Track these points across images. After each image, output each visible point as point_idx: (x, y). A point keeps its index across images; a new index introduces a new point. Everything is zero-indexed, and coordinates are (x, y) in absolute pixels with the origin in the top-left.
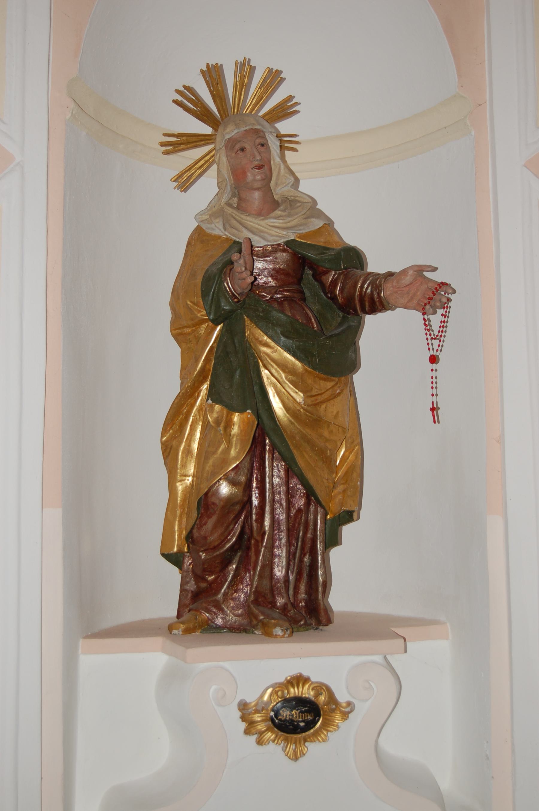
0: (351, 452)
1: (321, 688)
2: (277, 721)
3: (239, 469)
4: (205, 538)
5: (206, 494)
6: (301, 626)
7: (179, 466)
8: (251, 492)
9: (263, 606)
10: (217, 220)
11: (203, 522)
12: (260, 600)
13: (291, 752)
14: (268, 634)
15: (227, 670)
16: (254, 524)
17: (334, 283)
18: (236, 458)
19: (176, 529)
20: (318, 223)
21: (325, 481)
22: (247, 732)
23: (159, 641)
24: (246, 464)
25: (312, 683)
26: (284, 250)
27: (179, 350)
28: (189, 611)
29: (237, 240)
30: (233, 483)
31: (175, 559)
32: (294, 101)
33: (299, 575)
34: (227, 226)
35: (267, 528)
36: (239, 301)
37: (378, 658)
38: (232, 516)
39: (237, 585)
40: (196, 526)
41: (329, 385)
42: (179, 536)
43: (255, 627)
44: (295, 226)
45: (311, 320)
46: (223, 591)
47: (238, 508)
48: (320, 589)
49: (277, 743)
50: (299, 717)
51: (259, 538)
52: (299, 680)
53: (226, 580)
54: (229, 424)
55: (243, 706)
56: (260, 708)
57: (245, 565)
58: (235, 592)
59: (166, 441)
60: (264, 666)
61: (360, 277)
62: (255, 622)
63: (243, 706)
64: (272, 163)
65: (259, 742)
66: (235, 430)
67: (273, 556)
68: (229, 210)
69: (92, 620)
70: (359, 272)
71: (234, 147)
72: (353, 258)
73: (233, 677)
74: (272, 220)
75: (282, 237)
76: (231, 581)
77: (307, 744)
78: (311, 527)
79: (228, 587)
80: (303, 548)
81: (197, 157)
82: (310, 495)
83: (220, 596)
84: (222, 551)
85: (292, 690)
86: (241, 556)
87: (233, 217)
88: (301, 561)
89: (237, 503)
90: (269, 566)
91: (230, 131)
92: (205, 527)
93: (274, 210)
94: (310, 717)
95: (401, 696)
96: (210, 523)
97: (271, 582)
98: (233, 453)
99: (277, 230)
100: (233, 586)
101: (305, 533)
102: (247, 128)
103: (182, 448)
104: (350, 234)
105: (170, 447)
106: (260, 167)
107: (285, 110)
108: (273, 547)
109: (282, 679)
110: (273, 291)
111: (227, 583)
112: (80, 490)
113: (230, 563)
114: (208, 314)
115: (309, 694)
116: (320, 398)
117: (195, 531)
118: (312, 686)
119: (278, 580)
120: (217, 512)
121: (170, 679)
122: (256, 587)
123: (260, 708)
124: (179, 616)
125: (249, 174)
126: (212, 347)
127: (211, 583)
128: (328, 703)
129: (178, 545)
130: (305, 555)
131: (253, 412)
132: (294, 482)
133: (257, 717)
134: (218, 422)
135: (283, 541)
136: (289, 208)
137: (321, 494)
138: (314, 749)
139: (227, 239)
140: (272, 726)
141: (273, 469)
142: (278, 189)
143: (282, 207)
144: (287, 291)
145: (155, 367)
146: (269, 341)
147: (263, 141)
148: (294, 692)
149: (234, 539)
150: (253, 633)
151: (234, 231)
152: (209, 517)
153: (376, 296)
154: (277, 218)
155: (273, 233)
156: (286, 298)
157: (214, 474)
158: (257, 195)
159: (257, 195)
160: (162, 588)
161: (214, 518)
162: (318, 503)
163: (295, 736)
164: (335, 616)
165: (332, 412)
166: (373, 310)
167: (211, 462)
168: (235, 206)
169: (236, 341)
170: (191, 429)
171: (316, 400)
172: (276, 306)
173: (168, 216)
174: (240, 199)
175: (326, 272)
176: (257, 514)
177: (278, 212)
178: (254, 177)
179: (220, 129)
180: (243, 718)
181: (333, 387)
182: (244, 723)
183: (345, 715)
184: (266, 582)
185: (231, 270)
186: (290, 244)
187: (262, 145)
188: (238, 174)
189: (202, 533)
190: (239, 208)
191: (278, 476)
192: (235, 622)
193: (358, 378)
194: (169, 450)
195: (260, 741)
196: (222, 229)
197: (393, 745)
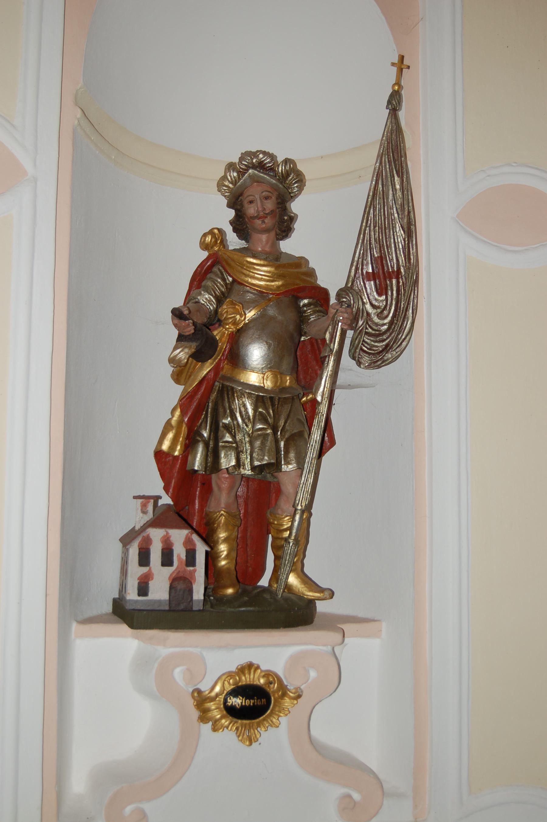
25: (262, 671)
49: (231, 730)
50: (252, 703)
52: (250, 667)
60: (222, 655)
65: (215, 729)
73: (204, 678)
79: (284, 460)
95: (348, 687)
109: (233, 669)
148: (246, 679)
164: (317, 614)
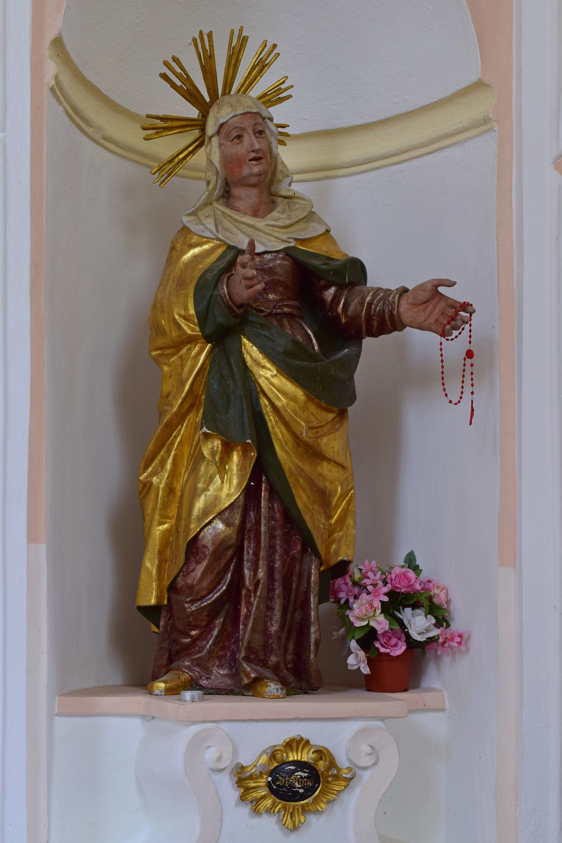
1: (321, 753)
2: (275, 787)
3: (233, 509)
9: (255, 664)
10: (209, 221)
11: (191, 568)
12: (252, 657)
20: (315, 230)
21: (321, 526)
22: (243, 798)
25: (312, 746)
29: (232, 244)
30: (227, 524)
33: (290, 632)
34: (220, 228)
40: (181, 574)
47: (230, 553)
51: (251, 588)
58: (220, 650)
60: (264, 725)
61: (368, 293)
72: (355, 271)
79: (214, 643)
89: (230, 547)
92: (193, 574)
100: (219, 642)
101: (298, 585)
105: (148, 485)
107: (275, 96)
110: (271, 306)
113: (216, 616)
117: (179, 579)
120: (208, 557)
128: (329, 768)
136: (288, 210)
144: (287, 306)
149: (224, 588)
151: (228, 233)
152: (198, 562)
161: (204, 564)
163: (293, 804)
165: (333, 447)
169: (232, 361)
171: (317, 433)
172: (275, 323)
184: (258, 637)
185: (229, 278)
187: (261, 132)
189: (189, 581)
194: (147, 488)
195: (255, 809)
196: (215, 231)
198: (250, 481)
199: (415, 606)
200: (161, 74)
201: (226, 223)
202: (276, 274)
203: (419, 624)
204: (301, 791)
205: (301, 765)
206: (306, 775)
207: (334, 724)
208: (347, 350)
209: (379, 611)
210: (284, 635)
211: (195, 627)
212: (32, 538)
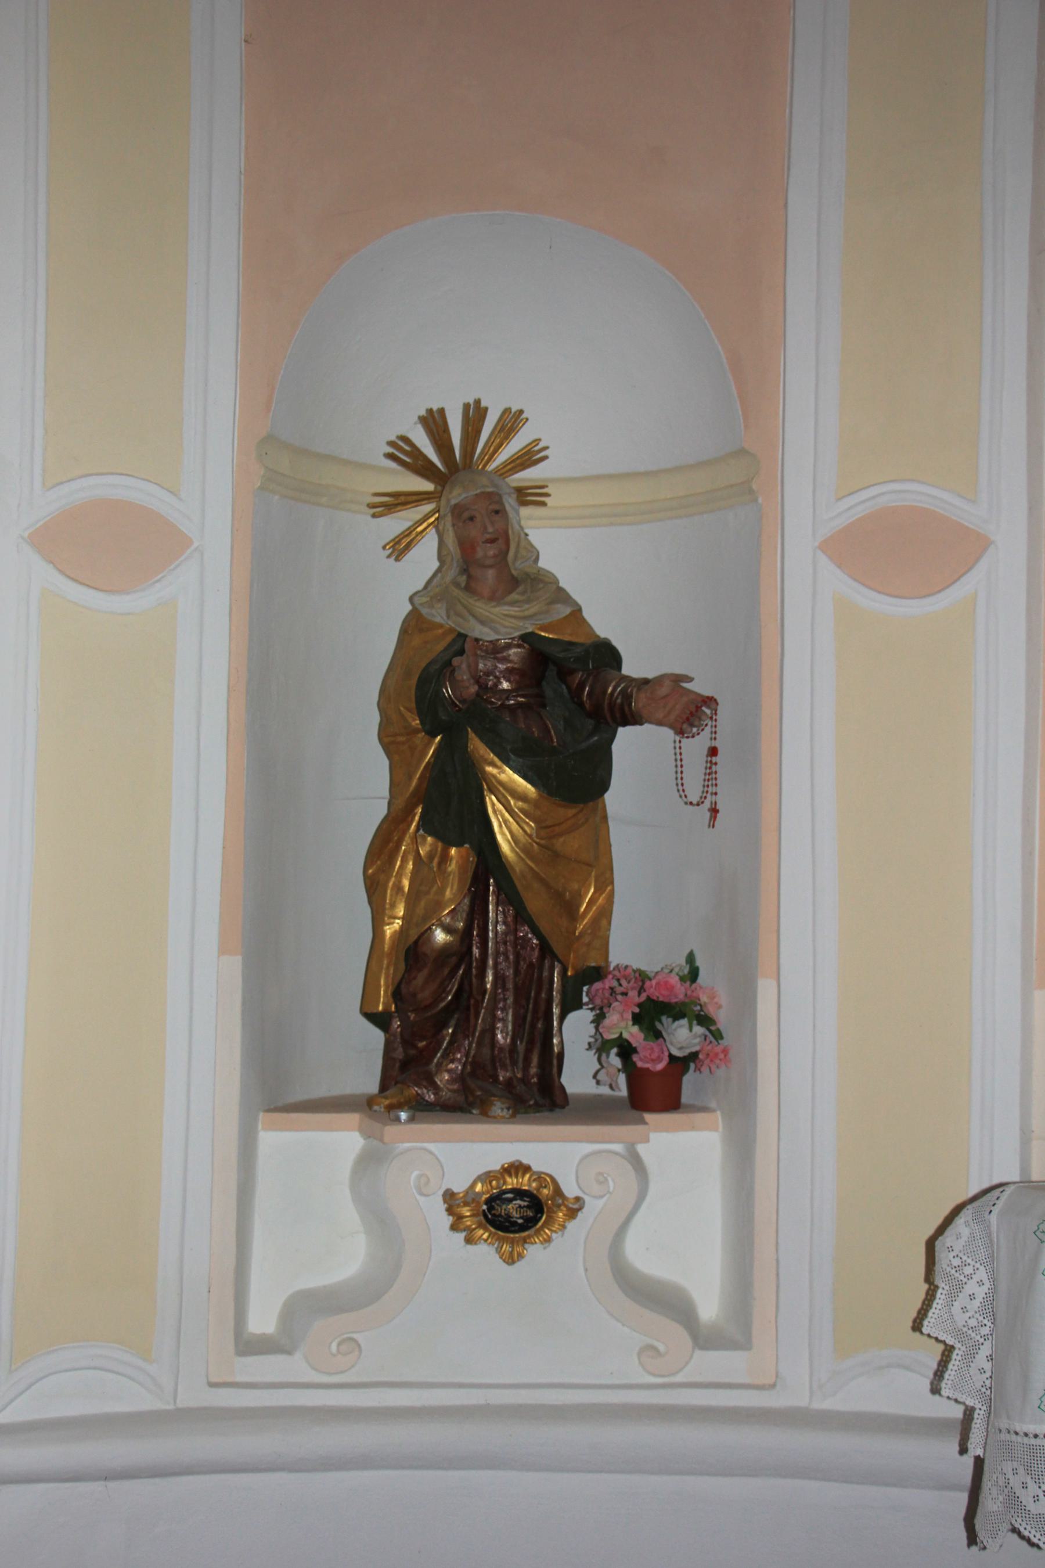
0: (601, 894)
4: (414, 995)
5: (416, 942)
6: (530, 1106)
7: (387, 906)
8: (471, 940)
10: (439, 605)
13: (507, 1255)
14: (485, 1115)
15: (431, 1153)
16: (474, 980)
17: (581, 686)
18: (451, 901)
19: (382, 982)
22: (454, 1227)
23: (354, 1118)
24: (465, 908)
26: (519, 646)
27: (387, 762)
28: (396, 1084)
29: (462, 631)
30: (447, 930)
31: (379, 1020)
32: (541, 445)
33: (531, 1043)
35: (488, 986)
36: (460, 709)
37: (618, 1147)
38: (446, 971)
39: (454, 1054)
41: (571, 812)
42: (386, 992)
43: (471, 1105)
44: (535, 615)
45: (549, 732)
46: (435, 1060)
47: (454, 960)
48: (555, 1062)
51: (479, 998)
52: (517, 1168)
53: (440, 1048)
54: (445, 858)
55: (449, 1196)
56: (469, 1199)
57: (464, 1029)
59: (373, 874)
60: (473, 1152)
62: (471, 1099)
63: (449, 1196)
64: (510, 531)
65: (469, 1241)
66: (452, 867)
67: (494, 1018)
68: (456, 592)
69: (277, 1092)
70: (614, 672)
71: (461, 515)
72: (607, 655)
74: (506, 608)
75: (516, 629)
76: (446, 1049)
77: (526, 1246)
78: (545, 987)
79: (442, 1056)
80: (535, 1011)
81: (419, 517)
82: (546, 949)
83: (433, 1067)
84: (434, 1011)
85: (509, 1180)
86: (458, 1019)
87: (460, 602)
88: (533, 1026)
90: (490, 1031)
91: (457, 495)
93: (510, 593)
94: (530, 1214)
96: (420, 978)
97: (493, 1050)
98: (448, 893)
99: (513, 621)
102: (478, 491)
103: (391, 884)
104: (603, 623)
106: (492, 541)
107: (529, 458)
108: (495, 1008)
110: (504, 696)
111: (441, 1051)
112: (264, 929)
113: (445, 1026)
114: (422, 723)
115: (530, 1185)
116: (557, 829)
117: (403, 986)
118: (535, 1177)
119: (501, 1049)
121: (368, 1163)
122: (474, 1056)
123: (469, 1199)
124: (384, 1087)
125: (479, 549)
126: (428, 763)
127: (421, 1051)
128: (553, 1199)
129: (384, 1003)
130: (538, 1019)
131: (472, 847)
132: (524, 931)
133: (466, 1212)
134: (431, 856)
135: (510, 1001)
137: (558, 948)
138: (534, 1252)
139: (451, 630)
140: (484, 1221)
141: (497, 915)
142: (518, 564)
143: (521, 589)
145: (362, 784)
146: (496, 759)
147: (496, 507)
148: (511, 1182)
150: (471, 1113)
151: (460, 620)
153: (626, 709)
154: (512, 604)
155: (507, 624)
156: (519, 705)
157: (425, 918)
158: (491, 573)
159: (491, 573)
160: (360, 1055)
161: (425, 972)
162: (555, 957)
166: (625, 724)
167: (423, 903)
168: (463, 585)
170: (402, 861)
173: (384, 582)
174: (469, 577)
175: (572, 672)
176: (477, 968)
177: (514, 596)
178: (486, 552)
179: (447, 488)
180: (450, 1211)
181: (574, 815)
182: (451, 1218)
183: (573, 1214)
184: (486, 1051)
186: (527, 638)
187: (497, 512)
188: (467, 548)
190: (468, 589)
191: (505, 923)
192: (449, 1099)
193: (611, 799)
197: (643, 1255)
198: (471, 885)
199: (676, 1017)
200: (478, 402)
201: (459, 607)
202: (511, 661)
203: (682, 1036)
204: (520, 1221)
205: (519, 1193)
206: (526, 1204)
207: (552, 1152)
208: (596, 738)
209: (630, 1023)
210: (521, 1047)
211: (422, 1039)
212: (223, 950)
